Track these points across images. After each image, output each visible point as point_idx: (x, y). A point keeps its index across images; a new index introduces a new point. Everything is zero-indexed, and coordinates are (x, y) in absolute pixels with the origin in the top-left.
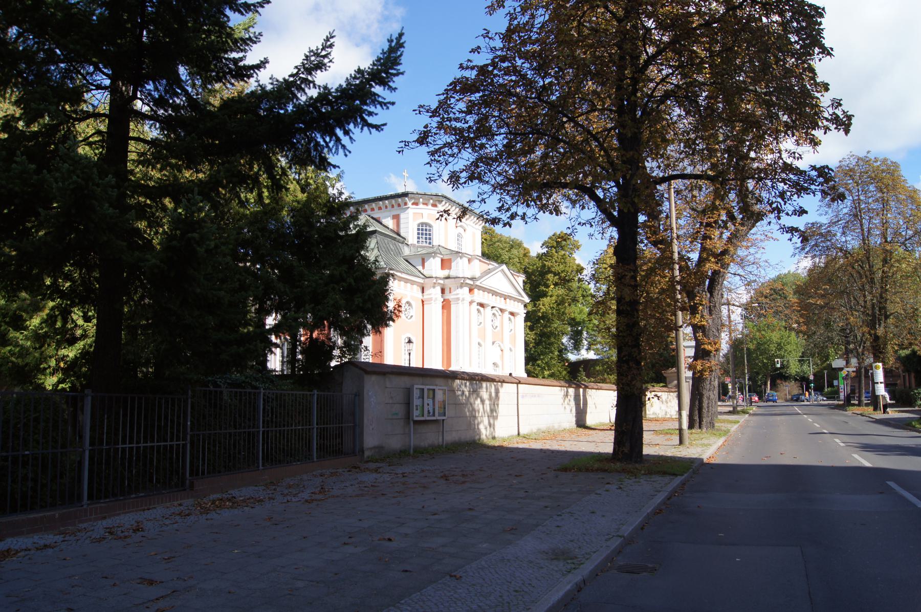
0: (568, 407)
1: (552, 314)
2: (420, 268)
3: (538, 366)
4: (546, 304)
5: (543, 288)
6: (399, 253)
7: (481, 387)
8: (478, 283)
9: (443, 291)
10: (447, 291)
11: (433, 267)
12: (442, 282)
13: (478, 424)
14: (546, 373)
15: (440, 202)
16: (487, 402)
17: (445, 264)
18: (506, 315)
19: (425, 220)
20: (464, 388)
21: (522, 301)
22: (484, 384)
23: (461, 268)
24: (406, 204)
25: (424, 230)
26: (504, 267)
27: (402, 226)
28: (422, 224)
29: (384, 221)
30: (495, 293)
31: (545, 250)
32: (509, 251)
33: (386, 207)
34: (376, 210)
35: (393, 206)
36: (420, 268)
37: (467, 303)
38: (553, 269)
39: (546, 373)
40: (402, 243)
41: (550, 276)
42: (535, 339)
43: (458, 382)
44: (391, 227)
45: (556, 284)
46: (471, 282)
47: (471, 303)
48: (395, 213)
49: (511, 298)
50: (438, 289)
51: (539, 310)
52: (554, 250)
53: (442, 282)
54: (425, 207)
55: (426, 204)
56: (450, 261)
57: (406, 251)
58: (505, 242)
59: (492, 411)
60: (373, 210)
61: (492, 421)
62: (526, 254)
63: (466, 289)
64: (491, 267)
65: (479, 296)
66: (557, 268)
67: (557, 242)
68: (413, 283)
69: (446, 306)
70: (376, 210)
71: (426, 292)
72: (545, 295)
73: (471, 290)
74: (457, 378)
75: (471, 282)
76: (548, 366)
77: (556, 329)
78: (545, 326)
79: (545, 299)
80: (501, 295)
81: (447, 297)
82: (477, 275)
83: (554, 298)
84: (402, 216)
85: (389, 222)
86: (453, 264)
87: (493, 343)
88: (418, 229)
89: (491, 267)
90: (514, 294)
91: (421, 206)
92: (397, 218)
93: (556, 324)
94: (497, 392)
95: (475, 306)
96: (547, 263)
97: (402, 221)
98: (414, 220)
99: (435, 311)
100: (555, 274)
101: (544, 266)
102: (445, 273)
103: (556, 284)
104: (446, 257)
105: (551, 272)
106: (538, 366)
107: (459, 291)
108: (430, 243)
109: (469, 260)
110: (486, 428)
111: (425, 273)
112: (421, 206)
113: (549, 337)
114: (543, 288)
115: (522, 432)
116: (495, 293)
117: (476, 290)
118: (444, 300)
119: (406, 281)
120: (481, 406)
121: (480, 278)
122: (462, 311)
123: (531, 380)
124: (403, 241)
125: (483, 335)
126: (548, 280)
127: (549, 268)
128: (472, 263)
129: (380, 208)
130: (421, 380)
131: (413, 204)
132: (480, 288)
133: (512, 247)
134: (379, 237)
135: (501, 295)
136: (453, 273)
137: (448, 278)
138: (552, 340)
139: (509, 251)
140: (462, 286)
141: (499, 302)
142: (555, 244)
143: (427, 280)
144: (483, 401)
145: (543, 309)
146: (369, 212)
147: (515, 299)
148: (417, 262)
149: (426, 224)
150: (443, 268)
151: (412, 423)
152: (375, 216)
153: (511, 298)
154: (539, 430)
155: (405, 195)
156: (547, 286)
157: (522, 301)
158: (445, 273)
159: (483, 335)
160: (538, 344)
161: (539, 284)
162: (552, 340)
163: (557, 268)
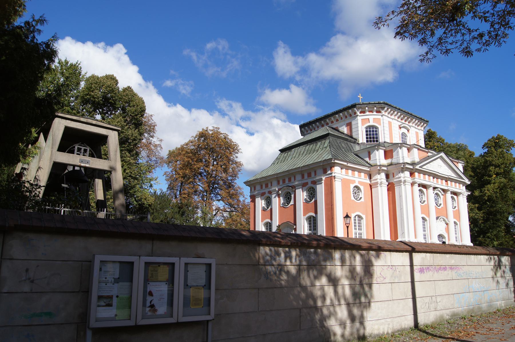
0: (501, 281)
1: (496, 197)
2: (367, 159)
3: (488, 237)
4: (490, 190)
5: (487, 178)
6: (350, 150)
7: (331, 258)
8: (417, 167)
9: (387, 176)
10: (391, 176)
11: (379, 157)
12: (385, 168)
13: (324, 319)
14: (496, 243)
15: (383, 108)
16: (345, 282)
17: (388, 154)
18: (449, 195)
19: (371, 123)
20: (291, 262)
21: (464, 183)
22: (337, 255)
23: (403, 156)
24: (355, 113)
25: (372, 134)
26: (442, 154)
27: (353, 130)
28: (370, 127)
29: (341, 129)
30: (435, 176)
31: (486, 150)
32: (457, 153)
33: (342, 118)
34: (335, 122)
35: (346, 117)
36: (367, 159)
37: (409, 186)
38: (494, 163)
39: (496, 243)
40: (354, 143)
41: (492, 168)
42: (484, 217)
43: (265, 250)
44: (346, 132)
45: (497, 174)
46: (411, 167)
47: (412, 184)
48: (348, 121)
49: (452, 180)
50: (383, 175)
51: (485, 195)
52: (493, 149)
53: (385, 168)
54: (371, 113)
55: (372, 112)
56: (391, 151)
57: (357, 148)
58: (453, 147)
59: (356, 295)
60: (332, 122)
61: (356, 311)
62: (471, 154)
63: (407, 174)
64: (429, 154)
65: (420, 178)
66: (497, 162)
67: (495, 143)
68: (360, 171)
69: (391, 188)
70: (335, 122)
71: (373, 178)
72: (489, 183)
73: (412, 174)
74: (260, 244)
75: (411, 167)
76: (497, 238)
77: (501, 208)
78: (492, 207)
79: (489, 186)
80: (442, 178)
81: (391, 181)
82: (417, 160)
83: (496, 184)
84: (353, 123)
85: (345, 130)
86: (394, 154)
87: (437, 218)
88: (367, 131)
89: (429, 154)
90: (453, 175)
91: (367, 113)
92: (349, 125)
93: (500, 205)
94: (368, 266)
95: (416, 188)
96: (488, 159)
97: (353, 127)
98: (363, 125)
99: (382, 192)
100: (496, 166)
101: (486, 161)
102: (389, 161)
103: (497, 174)
104: (388, 149)
105: (493, 165)
106: (488, 237)
107: (401, 175)
108: (377, 141)
109: (409, 150)
110: (343, 324)
111: (371, 162)
112: (367, 113)
113: (495, 215)
114: (487, 178)
115: (422, 320)
116: (435, 176)
117: (416, 174)
118: (389, 184)
119: (354, 169)
120: (330, 291)
121: (419, 163)
122: (407, 192)
123: (480, 249)
124: (355, 141)
125: (426, 210)
126: (490, 171)
127: (490, 162)
128: (411, 152)
129: (337, 120)
130: (147, 246)
131: (360, 113)
132: (420, 172)
133: (458, 150)
134: (331, 138)
135: (442, 178)
136: (394, 161)
137: (391, 164)
138: (499, 217)
139: (457, 153)
140: (403, 170)
141: (441, 184)
142: (494, 144)
143: (372, 168)
144: (334, 281)
145: (488, 193)
146: (330, 124)
147: (456, 181)
148: (364, 155)
149: (373, 127)
150: (386, 157)
151: (89, 334)
152: (334, 126)
153: (452, 180)
154: (454, 315)
155: (354, 106)
156: (490, 176)
157: (464, 183)
158: (389, 161)
159: (426, 210)
160: (486, 220)
161: (483, 175)
162: (499, 217)
163: (497, 162)
